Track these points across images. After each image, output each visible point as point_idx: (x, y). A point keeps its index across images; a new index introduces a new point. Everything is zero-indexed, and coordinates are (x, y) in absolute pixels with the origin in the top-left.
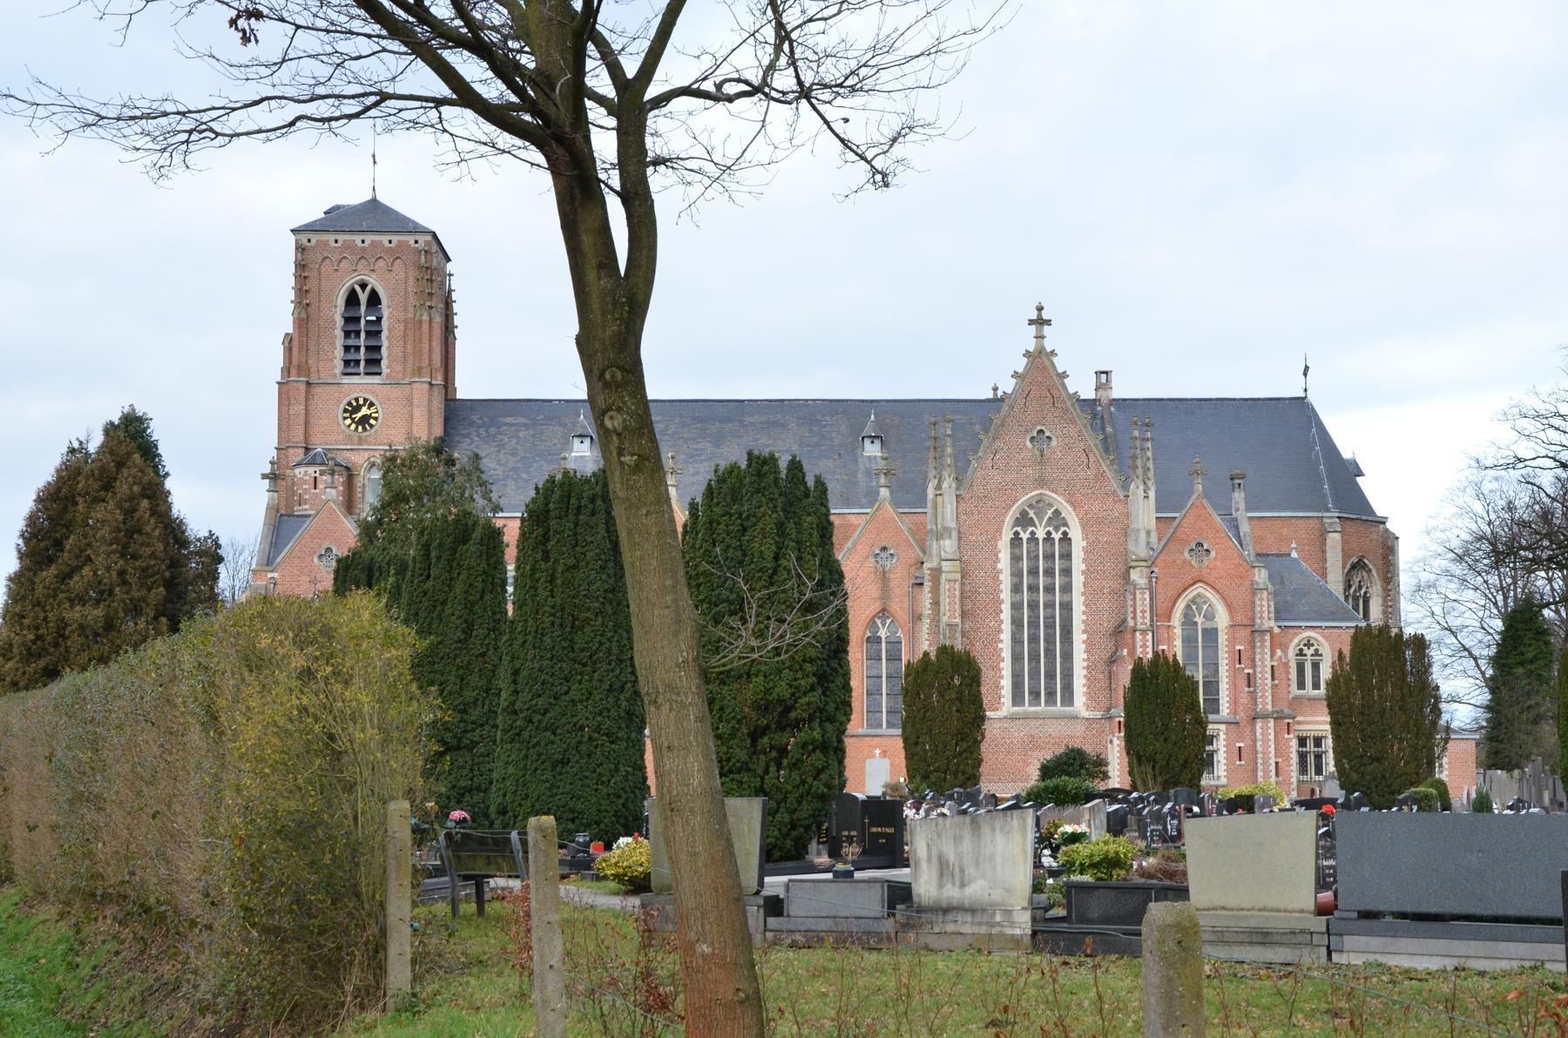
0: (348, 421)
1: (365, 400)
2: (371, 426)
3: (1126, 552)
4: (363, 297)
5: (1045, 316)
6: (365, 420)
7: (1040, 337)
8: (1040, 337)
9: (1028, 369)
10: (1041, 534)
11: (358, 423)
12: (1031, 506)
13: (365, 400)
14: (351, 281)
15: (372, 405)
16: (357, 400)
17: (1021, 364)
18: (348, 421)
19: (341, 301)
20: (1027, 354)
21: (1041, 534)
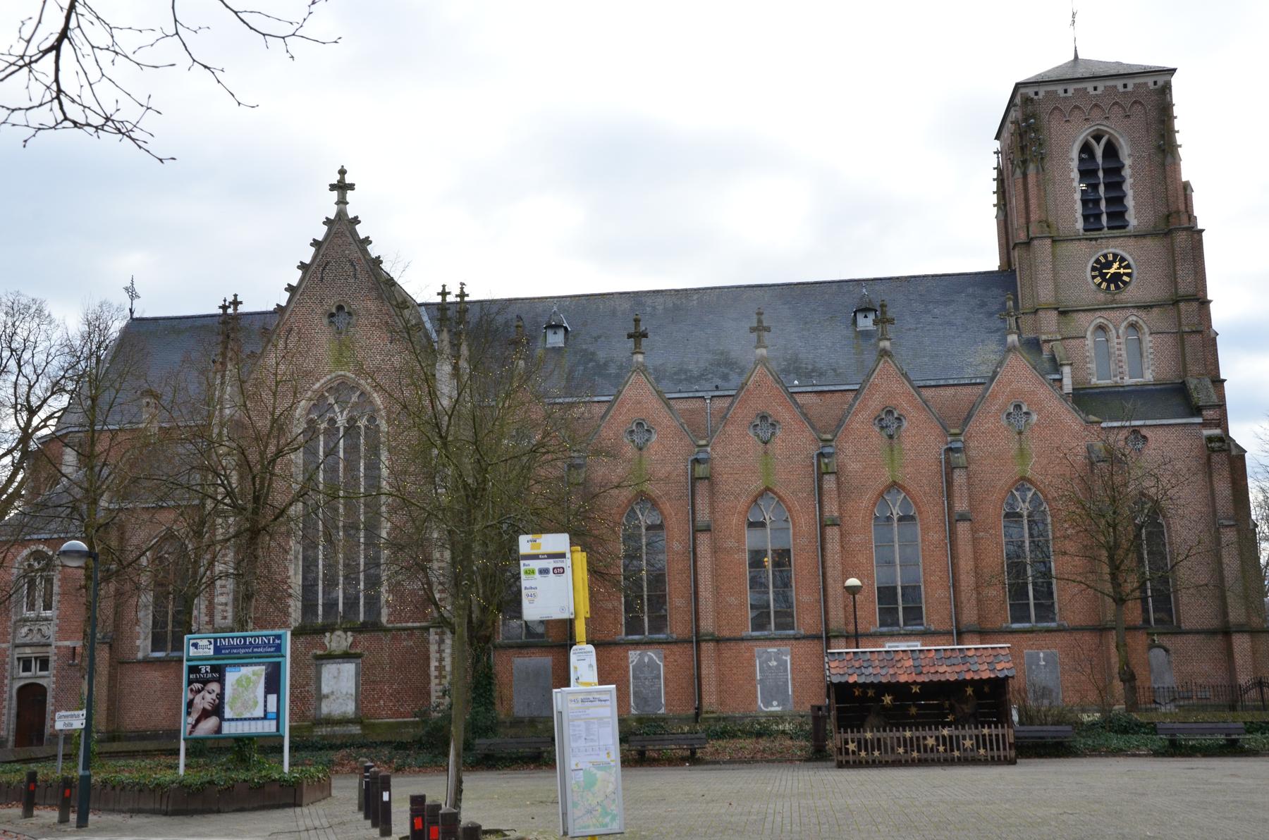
0: (1098, 280)
1: (1115, 256)
2: (1125, 283)
3: (333, 631)
4: (1099, 151)
5: (348, 180)
6: (1117, 277)
7: (342, 202)
8: (342, 202)
9: (354, 234)
10: (341, 421)
11: (1109, 282)
12: (362, 393)
13: (1115, 256)
14: (1083, 135)
15: (1128, 266)
16: (1105, 256)
17: (320, 232)
18: (1098, 280)
19: (1075, 154)
20: (328, 222)
21: (341, 421)
